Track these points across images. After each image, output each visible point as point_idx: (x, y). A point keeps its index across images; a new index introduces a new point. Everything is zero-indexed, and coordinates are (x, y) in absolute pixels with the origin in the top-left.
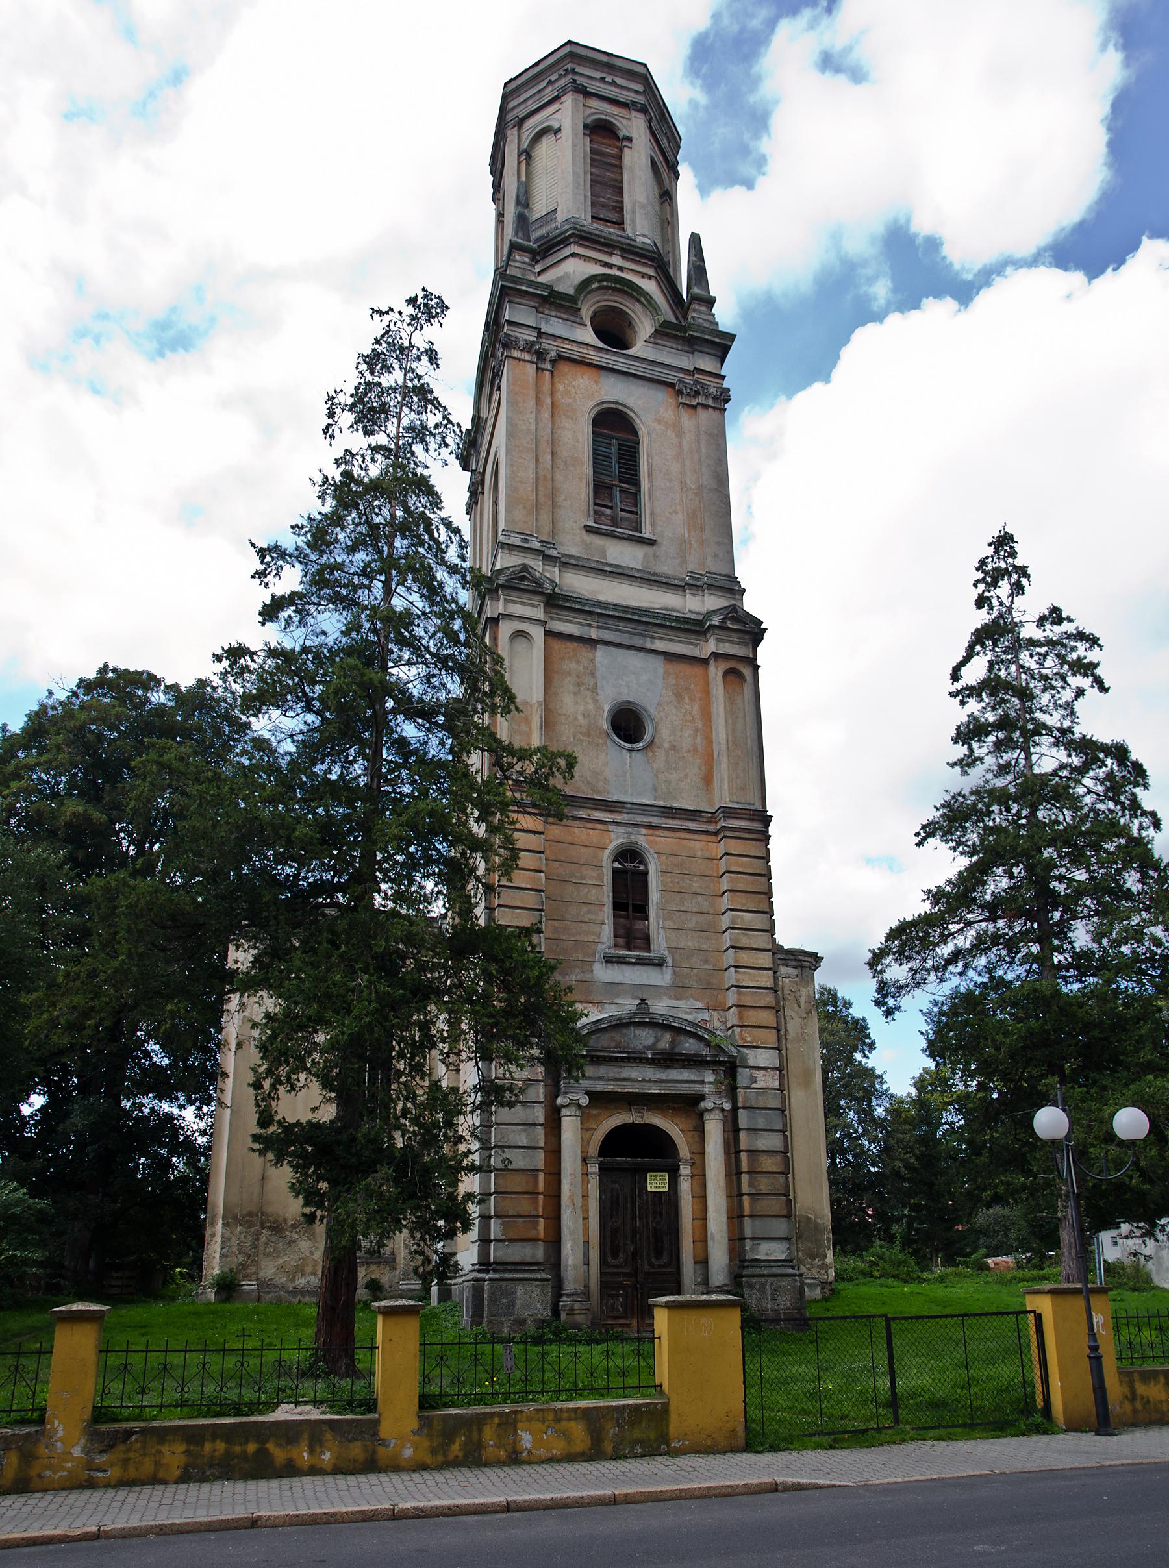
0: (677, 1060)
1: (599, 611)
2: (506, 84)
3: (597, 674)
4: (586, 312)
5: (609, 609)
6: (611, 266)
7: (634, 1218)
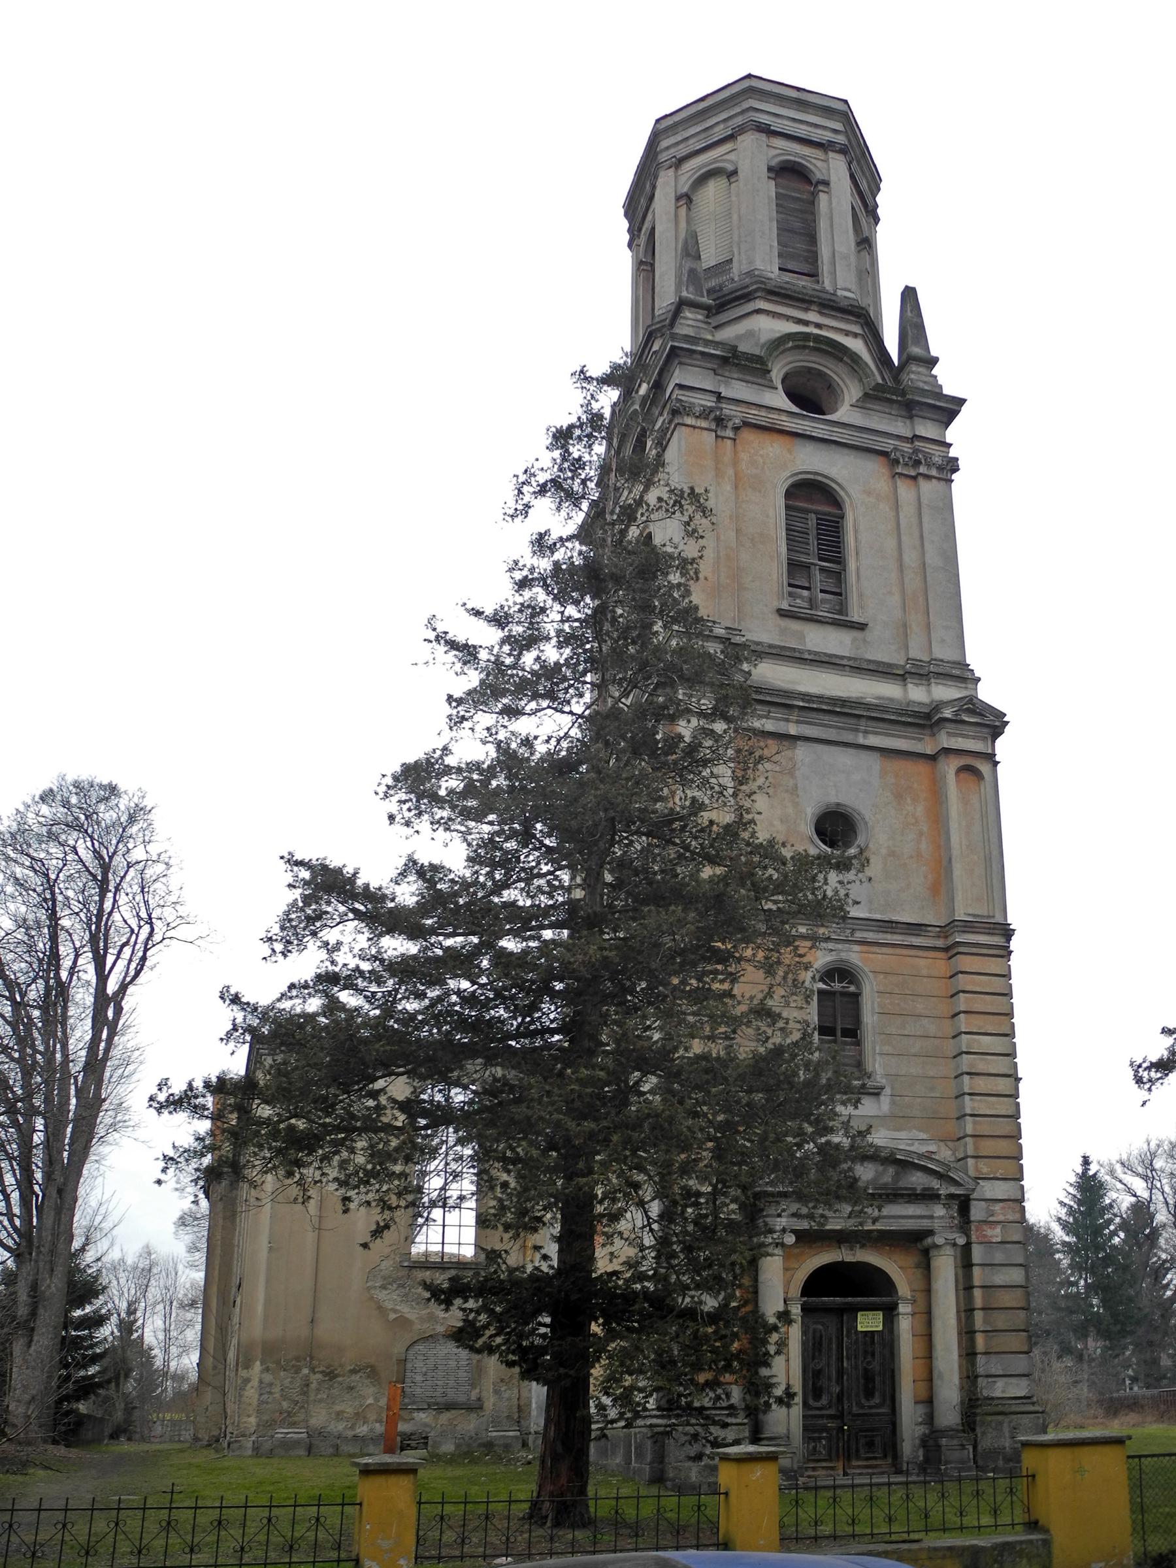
0: (902, 1195)
1: (801, 704)
2: (658, 121)
3: (797, 773)
4: (777, 374)
5: (813, 702)
6: (806, 323)
7: (840, 1359)
